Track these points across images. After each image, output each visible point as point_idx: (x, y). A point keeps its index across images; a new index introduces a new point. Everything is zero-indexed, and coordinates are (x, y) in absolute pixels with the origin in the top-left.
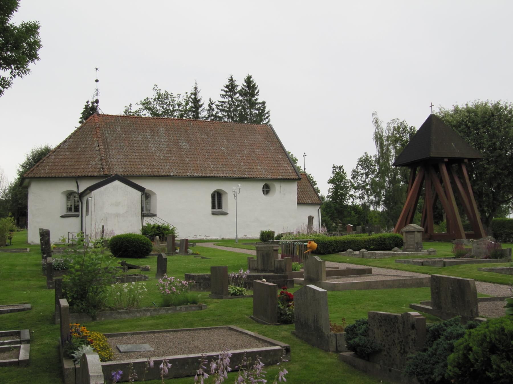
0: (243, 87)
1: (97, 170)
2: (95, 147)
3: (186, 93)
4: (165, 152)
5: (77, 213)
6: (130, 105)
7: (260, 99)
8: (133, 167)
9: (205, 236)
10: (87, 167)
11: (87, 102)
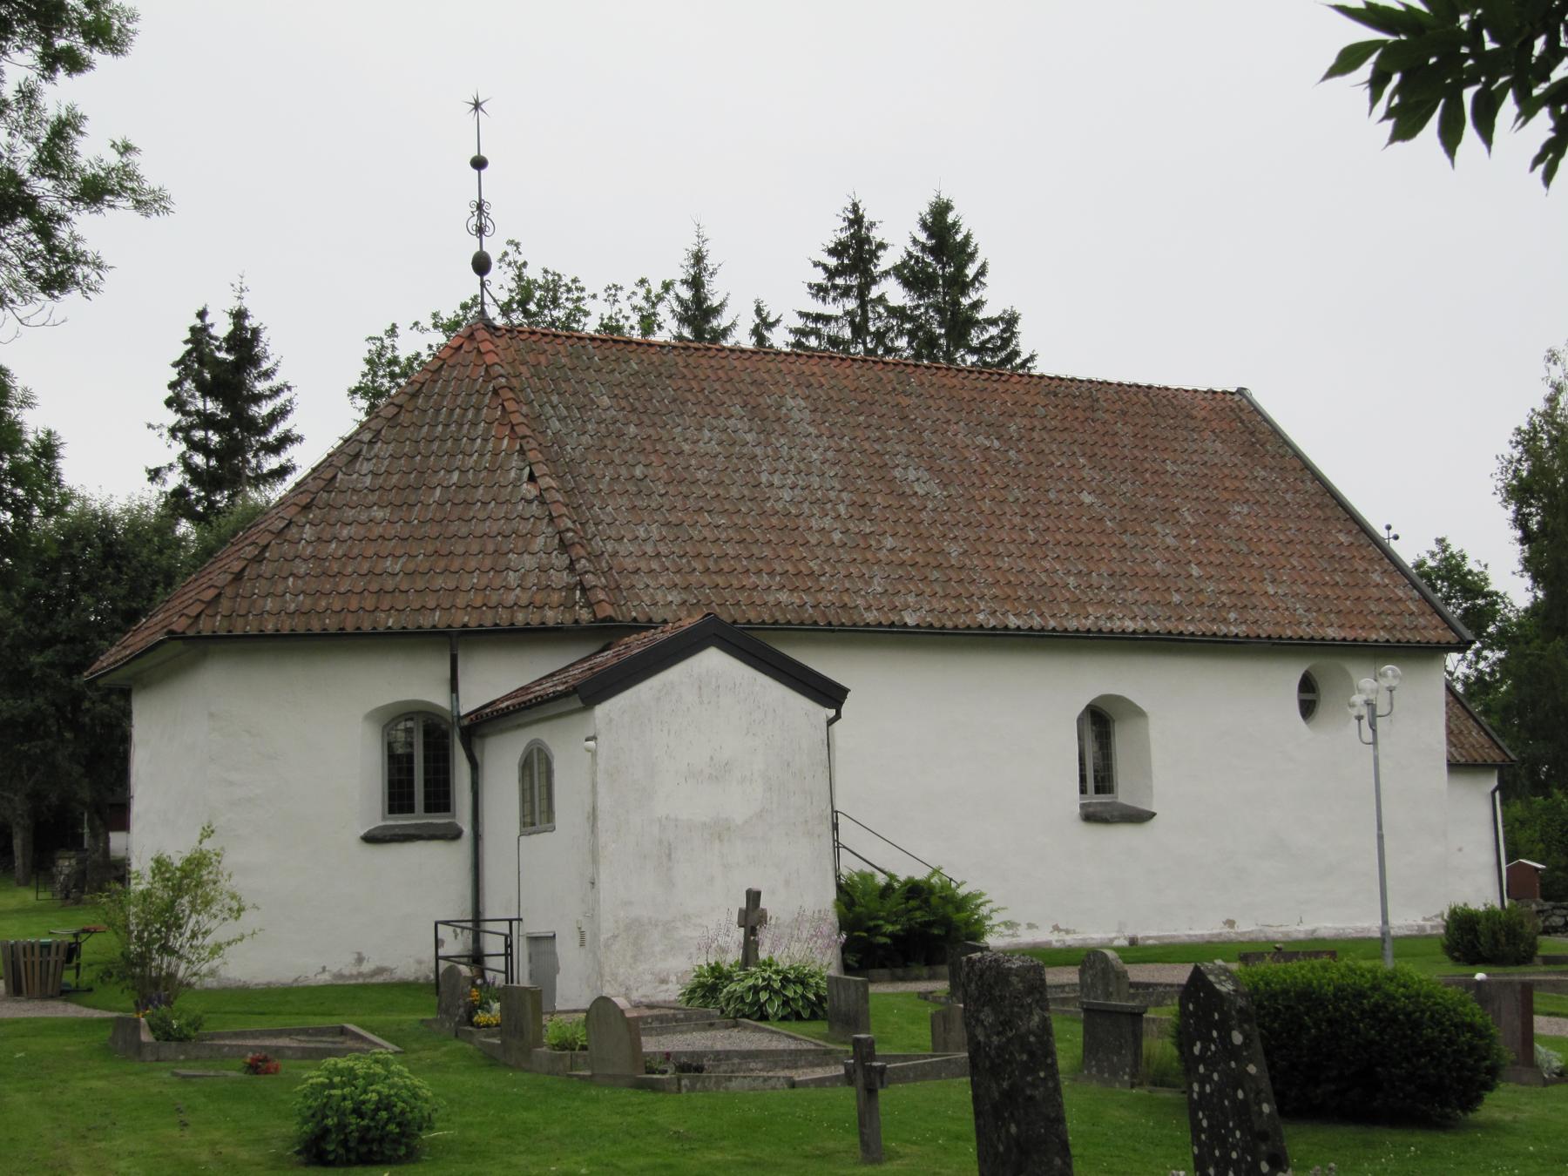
0: (917, 252)
1: (555, 598)
2: (516, 485)
3: (643, 282)
4: (842, 509)
5: (438, 819)
6: (392, 332)
7: (993, 298)
8: (720, 581)
9: (1056, 928)
10: (498, 583)
11: (202, 315)
